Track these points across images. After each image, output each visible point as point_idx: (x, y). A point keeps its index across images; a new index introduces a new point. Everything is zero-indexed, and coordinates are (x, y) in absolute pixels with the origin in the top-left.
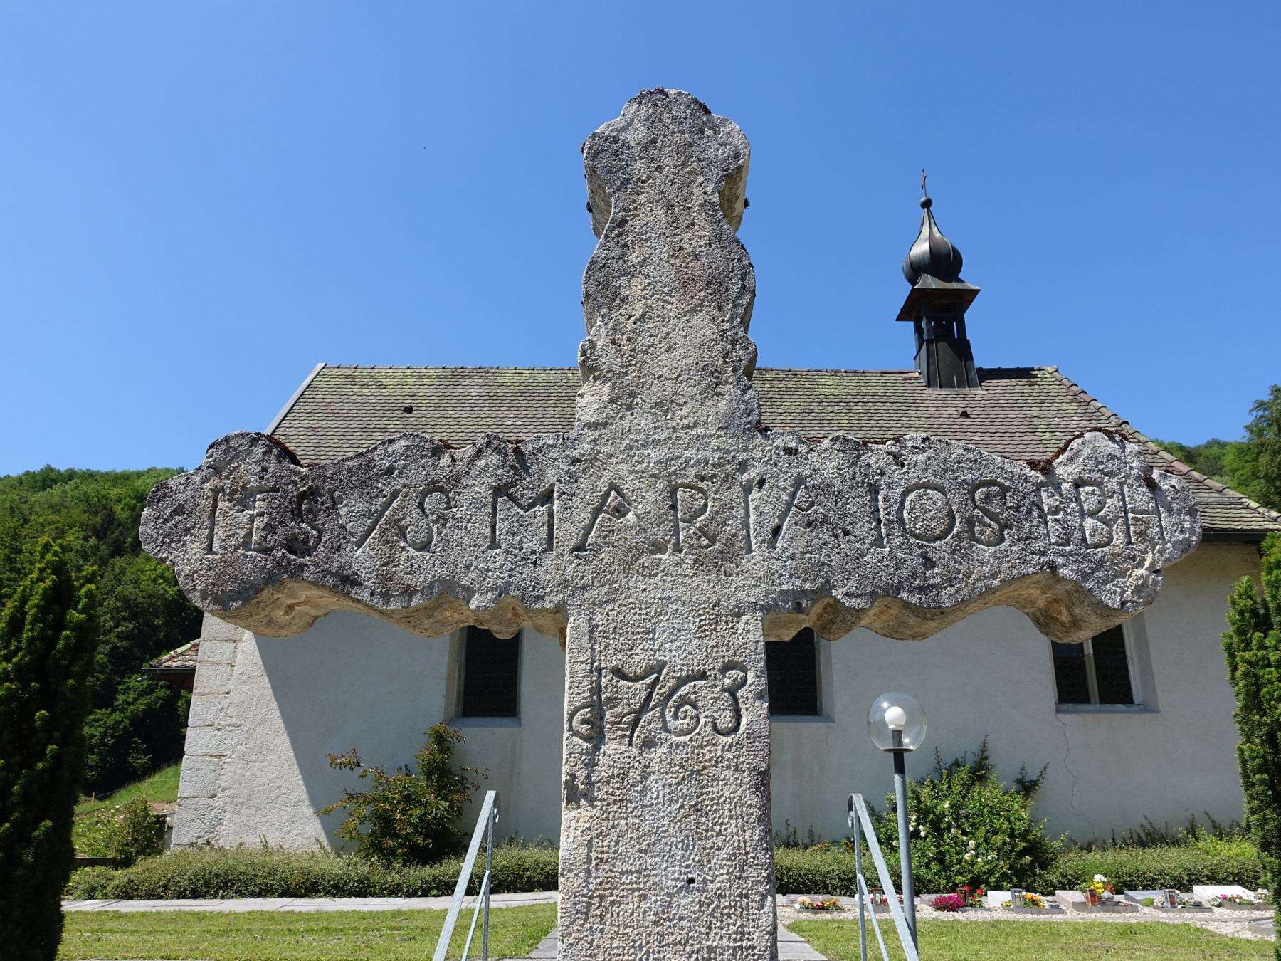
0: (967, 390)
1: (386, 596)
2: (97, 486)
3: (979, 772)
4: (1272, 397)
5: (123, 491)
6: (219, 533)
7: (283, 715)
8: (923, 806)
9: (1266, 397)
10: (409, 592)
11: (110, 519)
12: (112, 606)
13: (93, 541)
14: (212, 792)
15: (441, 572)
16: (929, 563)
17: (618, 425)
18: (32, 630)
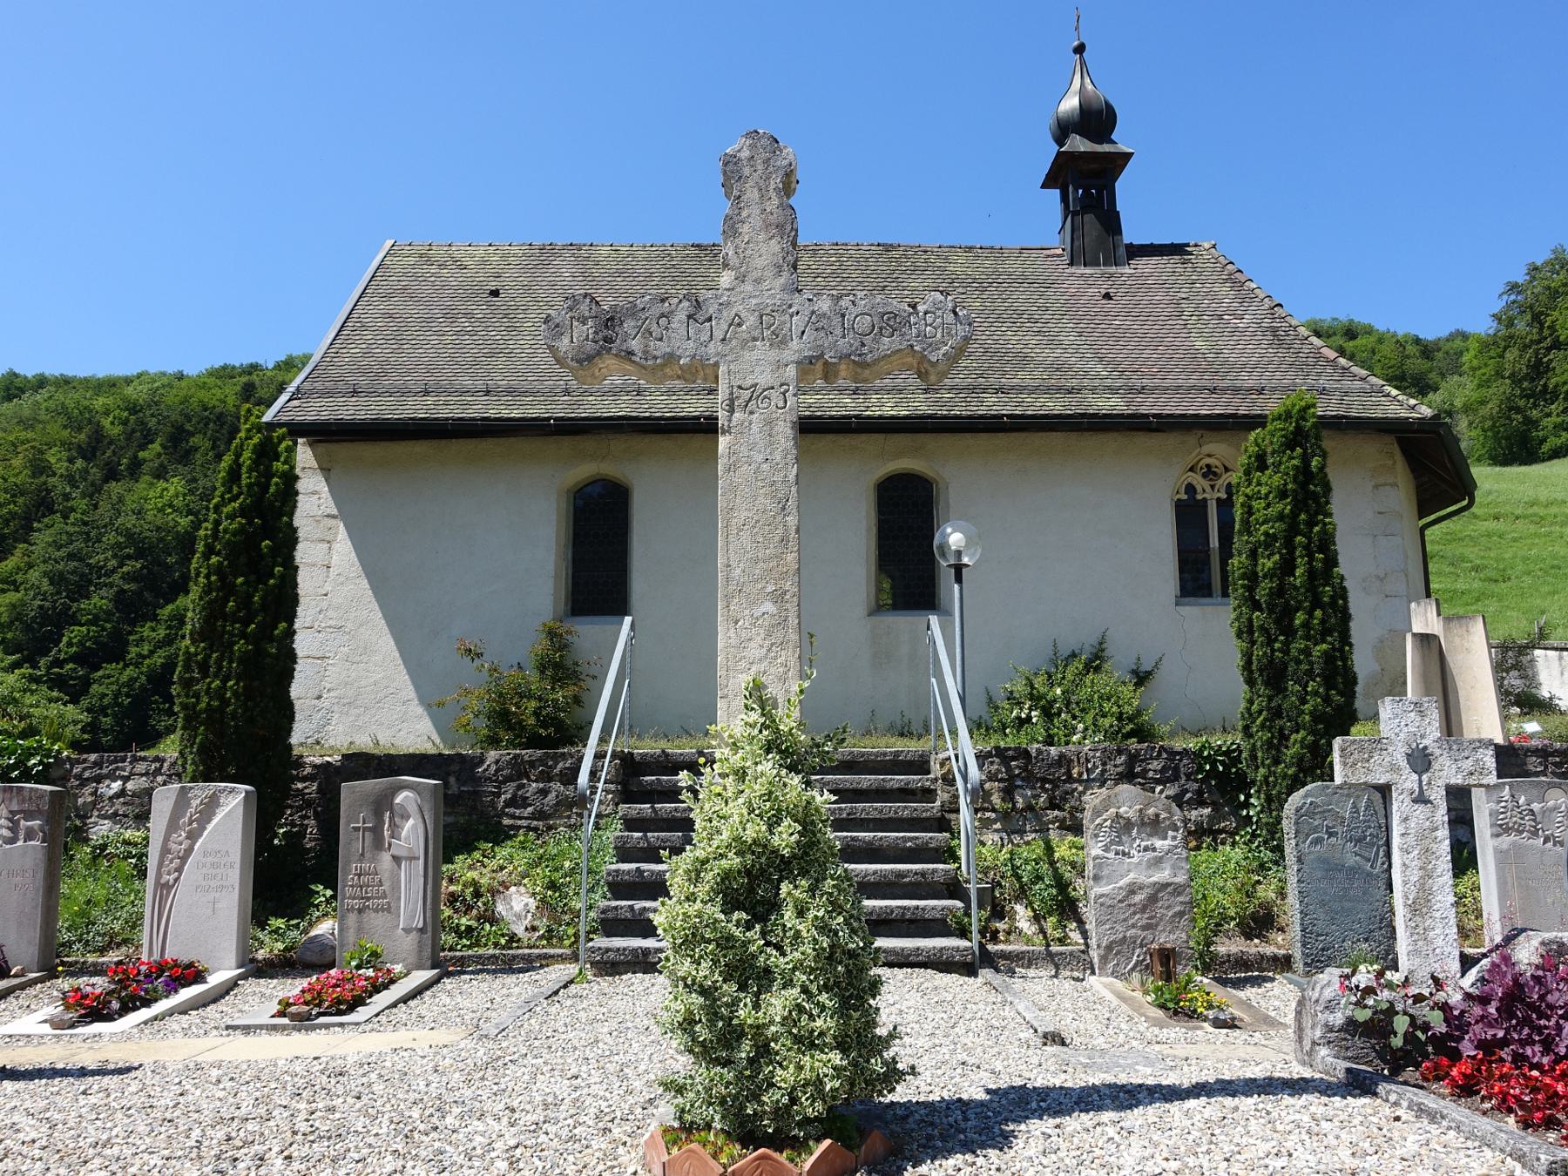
0: (1113, 269)
1: (646, 359)
2: (76, 396)
3: (1095, 662)
4: (1528, 278)
5: (110, 401)
6: (575, 335)
7: (385, 616)
8: (1035, 692)
9: (1521, 277)
10: (655, 358)
11: (98, 436)
12: (112, 541)
13: (80, 463)
14: (317, 693)
15: (668, 350)
16: (863, 345)
17: (738, 289)
18: (249, 478)
